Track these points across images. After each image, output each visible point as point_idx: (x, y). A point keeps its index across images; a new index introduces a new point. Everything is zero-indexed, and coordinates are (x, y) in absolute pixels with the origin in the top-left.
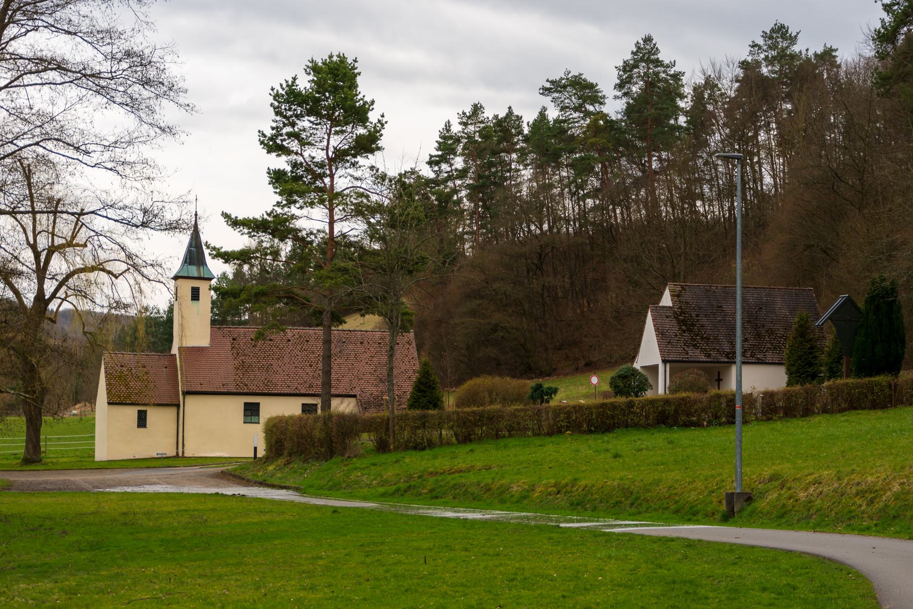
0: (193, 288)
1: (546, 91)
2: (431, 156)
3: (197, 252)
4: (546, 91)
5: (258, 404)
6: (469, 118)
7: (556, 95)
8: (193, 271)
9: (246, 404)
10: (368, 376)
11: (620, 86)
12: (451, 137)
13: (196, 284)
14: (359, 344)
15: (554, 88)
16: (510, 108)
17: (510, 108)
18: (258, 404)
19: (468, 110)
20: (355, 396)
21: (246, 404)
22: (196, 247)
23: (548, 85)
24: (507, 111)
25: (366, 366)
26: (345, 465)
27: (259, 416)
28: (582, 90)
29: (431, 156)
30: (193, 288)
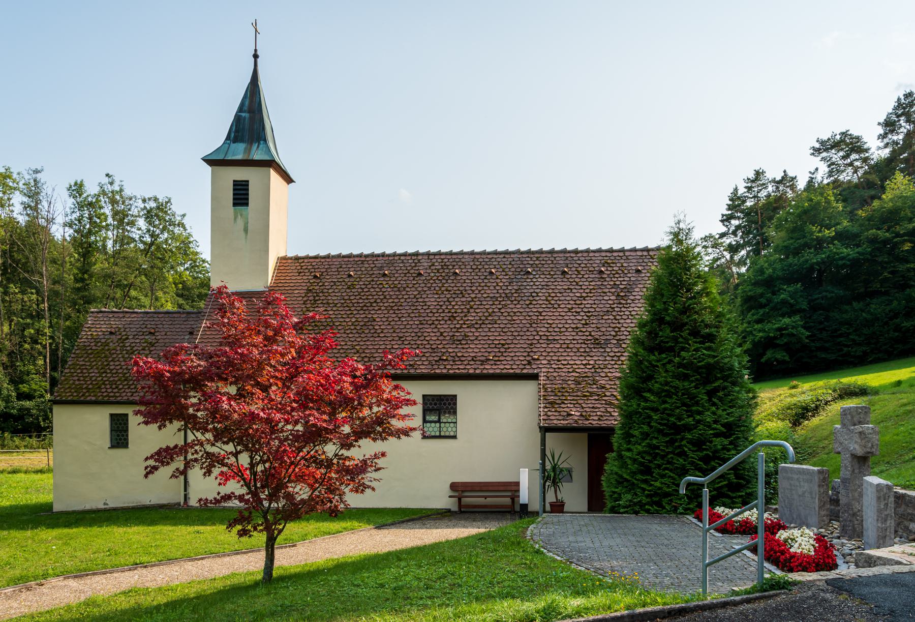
0: (236, 184)
1: (816, 151)
2: (723, 215)
3: (252, 119)
4: (816, 151)
5: (454, 397)
6: (753, 181)
7: (824, 154)
8: (238, 152)
9: (112, 415)
10: (570, 335)
11: (883, 137)
12: (739, 198)
13: (241, 174)
14: (559, 276)
15: (824, 147)
16: (785, 171)
17: (785, 171)
18: (454, 397)
19: (752, 175)
20: (535, 377)
21: (112, 415)
22: (250, 111)
23: (817, 145)
24: (783, 174)
25: (569, 317)
26: (487, 551)
27: (455, 413)
28: (849, 144)
29: (723, 215)
30: (236, 184)
